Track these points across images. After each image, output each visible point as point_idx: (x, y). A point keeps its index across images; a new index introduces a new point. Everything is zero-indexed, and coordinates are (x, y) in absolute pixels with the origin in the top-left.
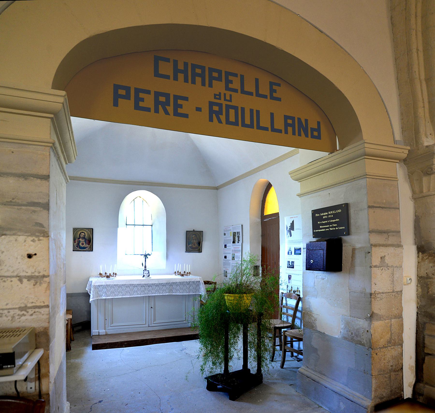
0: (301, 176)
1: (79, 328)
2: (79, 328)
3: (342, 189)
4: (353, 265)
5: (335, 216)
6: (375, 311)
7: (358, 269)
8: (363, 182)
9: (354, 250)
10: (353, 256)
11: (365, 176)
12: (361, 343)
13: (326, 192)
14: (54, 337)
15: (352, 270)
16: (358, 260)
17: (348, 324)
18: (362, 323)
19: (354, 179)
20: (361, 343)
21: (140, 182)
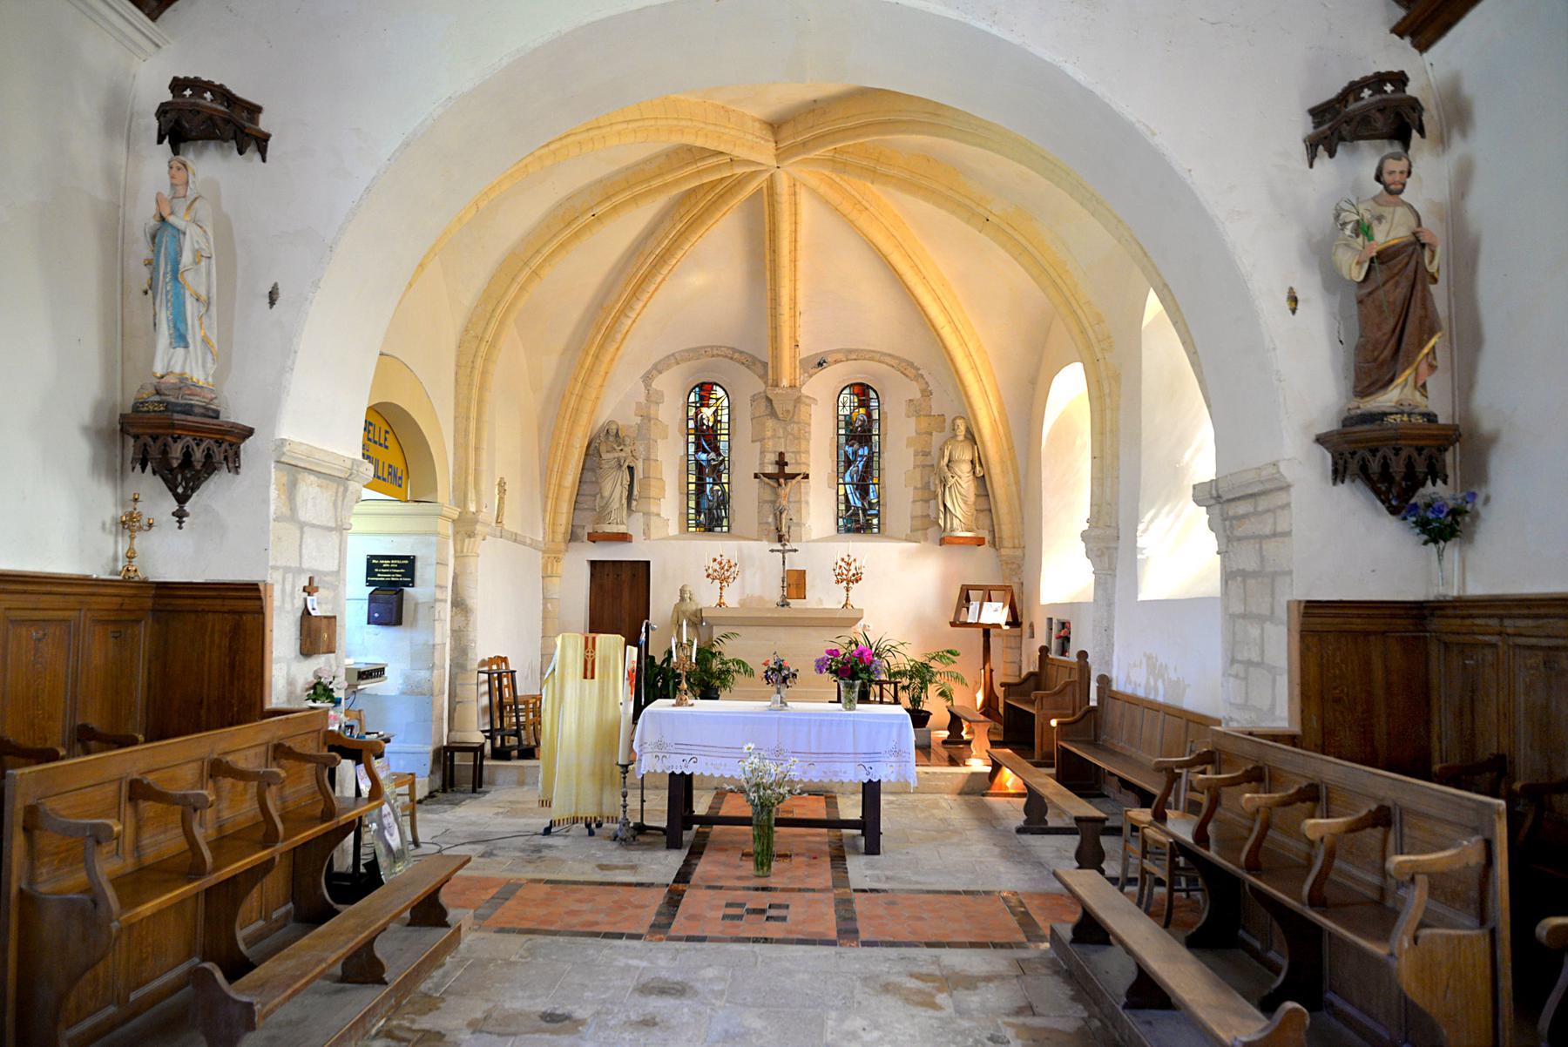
0: (1434, 484)
1: (206, 119)
2: (206, 119)
3: (412, 539)
4: (415, 619)
5: (400, 566)
6: (766, 545)
7: (421, 622)
8: (434, 539)
9: (416, 604)
10: (415, 611)
11: (437, 534)
12: (422, 694)
13: (388, 538)
14: (95, 464)
15: (414, 623)
16: (420, 615)
17: (407, 678)
18: (424, 674)
19: (426, 534)
20: (422, 694)
21: (662, 259)
